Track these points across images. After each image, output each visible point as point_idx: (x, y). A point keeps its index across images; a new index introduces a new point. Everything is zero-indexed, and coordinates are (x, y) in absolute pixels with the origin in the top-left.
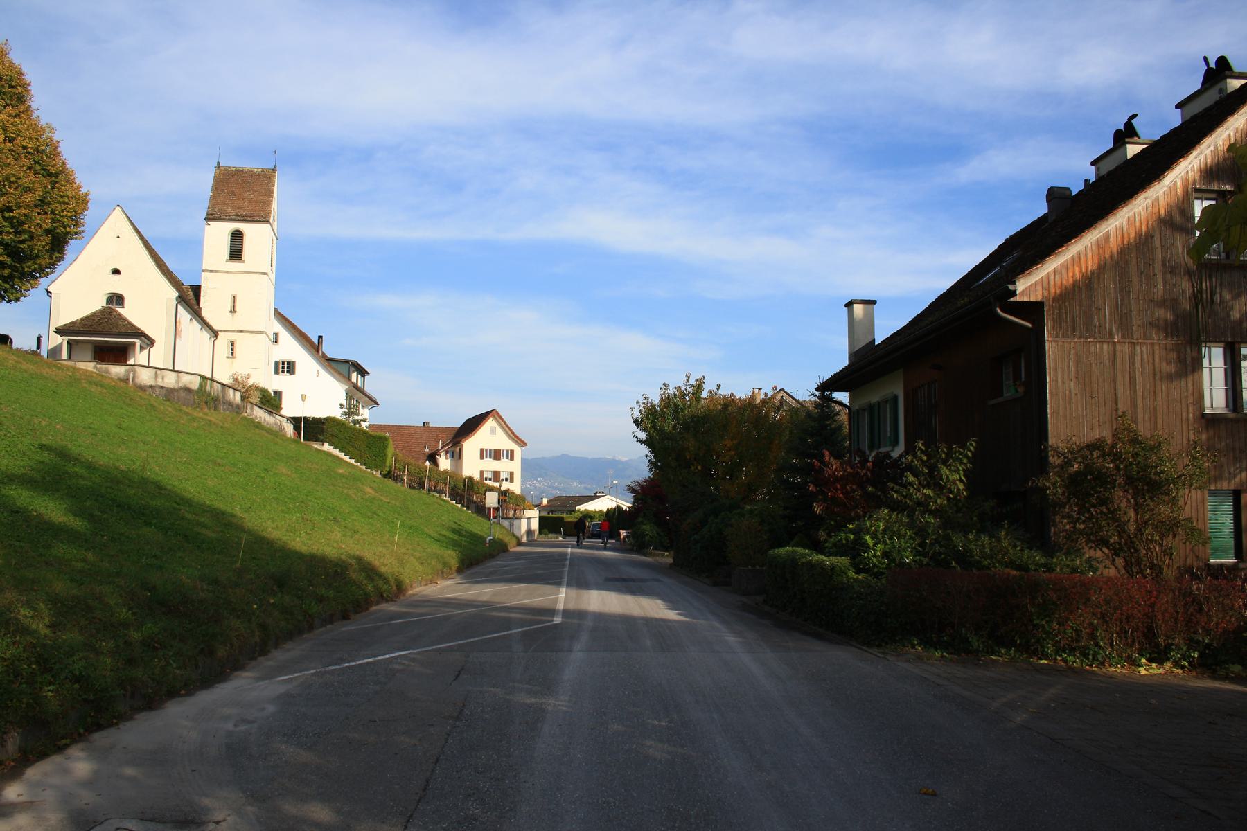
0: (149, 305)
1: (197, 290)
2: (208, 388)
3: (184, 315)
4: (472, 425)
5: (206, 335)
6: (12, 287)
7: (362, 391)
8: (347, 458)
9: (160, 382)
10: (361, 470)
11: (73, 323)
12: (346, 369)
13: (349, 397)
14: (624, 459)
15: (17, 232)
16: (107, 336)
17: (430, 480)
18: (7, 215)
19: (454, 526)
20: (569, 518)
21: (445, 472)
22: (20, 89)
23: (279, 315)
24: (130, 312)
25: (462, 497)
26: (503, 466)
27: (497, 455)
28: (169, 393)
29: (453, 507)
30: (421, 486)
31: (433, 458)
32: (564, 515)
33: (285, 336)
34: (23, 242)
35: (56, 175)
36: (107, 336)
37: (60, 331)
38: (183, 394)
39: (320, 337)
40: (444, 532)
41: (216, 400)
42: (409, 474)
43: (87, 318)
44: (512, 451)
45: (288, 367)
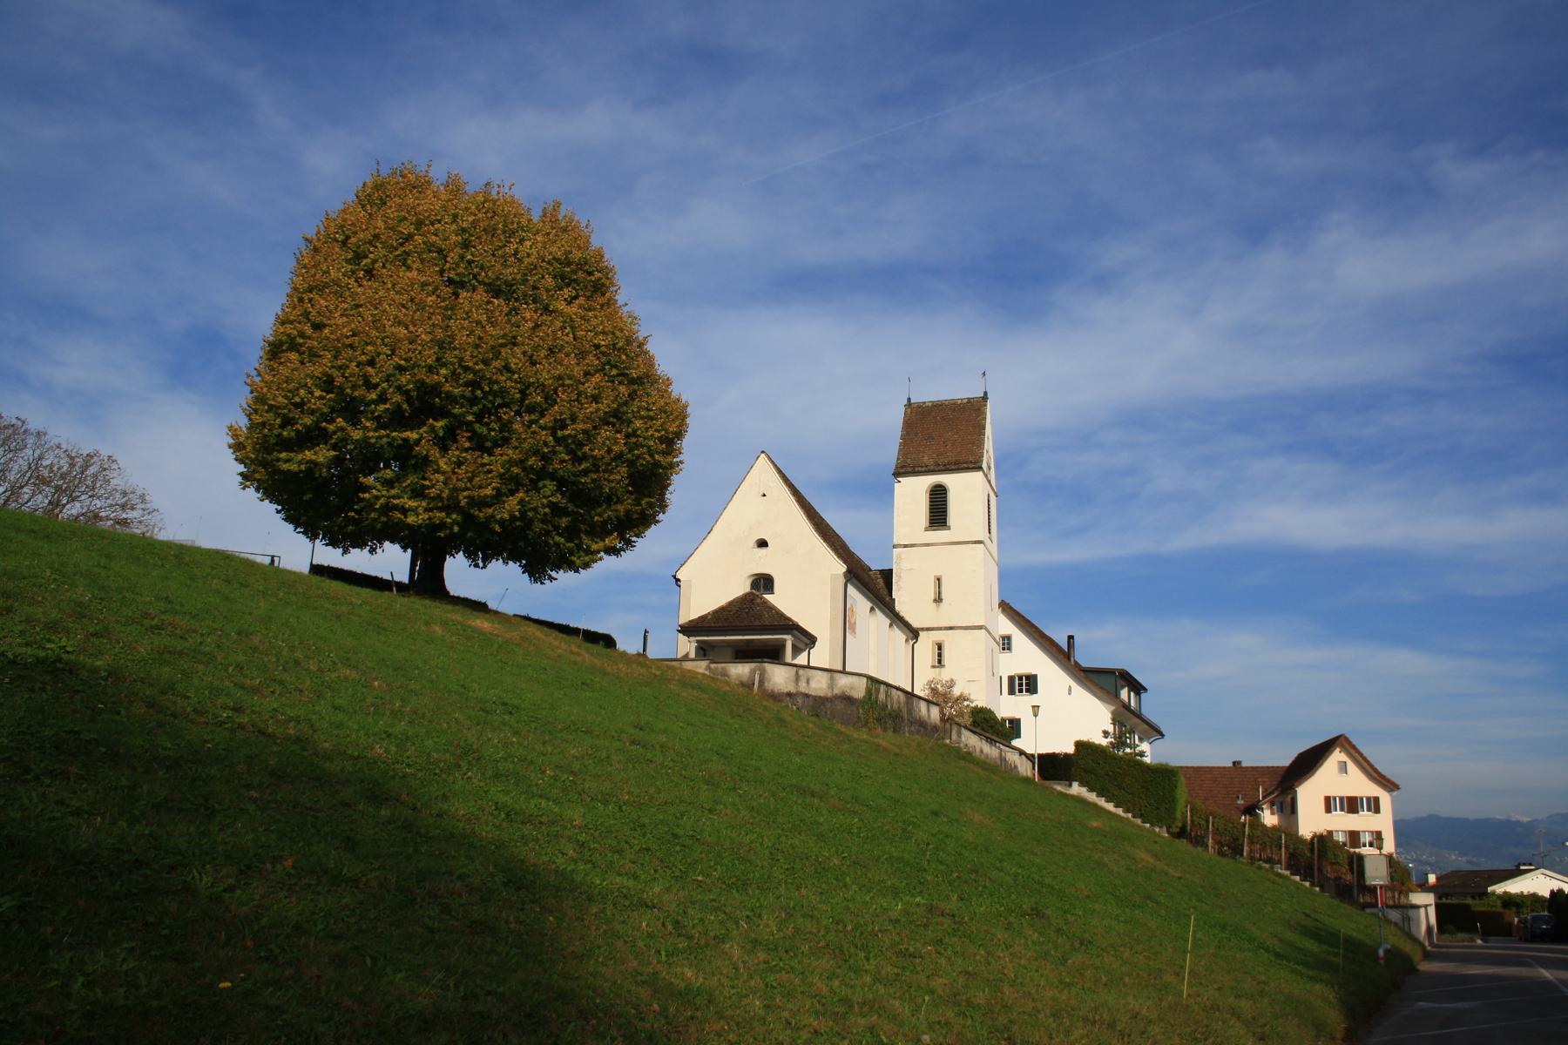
0: (809, 589)
1: (887, 575)
2: (882, 696)
3: (860, 603)
4: (1308, 762)
5: (899, 636)
6: (579, 547)
7: (1138, 715)
8: (1110, 807)
9: (803, 687)
10: (1134, 825)
11: (702, 618)
12: (1107, 681)
13: (1115, 721)
14: (1525, 819)
15: (577, 460)
16: (752, 626)
17: (1251, 842)
18: (560, 433)
19: (1308, 922)
20: (1478, 906)
21: (1274, 828)
22: (598, 275)
23: (1005, 607)
24: (778, 599)
25: (1310, 866)
26: (1362, 822)
27: (1352, 805)
28: (818, 705)
29: (1298, 887)
30: (1237, 850)
31: (1252, 810)
32: (1469, 901)
33: (1020, 639)
34: (586, 472)
35: (639, 381)
36: (752, 626)
37: (688, 629)
38: (840, 706)
39: (1071, 637)
40: (1291, 936)
41: (896, 717)
42: (1216, 832)
43: (722, 609)
44: (1377, 799)
45: (1028, 684)
